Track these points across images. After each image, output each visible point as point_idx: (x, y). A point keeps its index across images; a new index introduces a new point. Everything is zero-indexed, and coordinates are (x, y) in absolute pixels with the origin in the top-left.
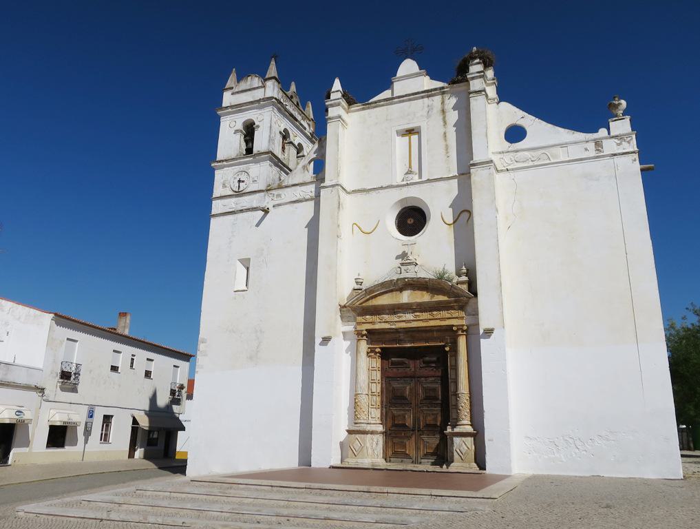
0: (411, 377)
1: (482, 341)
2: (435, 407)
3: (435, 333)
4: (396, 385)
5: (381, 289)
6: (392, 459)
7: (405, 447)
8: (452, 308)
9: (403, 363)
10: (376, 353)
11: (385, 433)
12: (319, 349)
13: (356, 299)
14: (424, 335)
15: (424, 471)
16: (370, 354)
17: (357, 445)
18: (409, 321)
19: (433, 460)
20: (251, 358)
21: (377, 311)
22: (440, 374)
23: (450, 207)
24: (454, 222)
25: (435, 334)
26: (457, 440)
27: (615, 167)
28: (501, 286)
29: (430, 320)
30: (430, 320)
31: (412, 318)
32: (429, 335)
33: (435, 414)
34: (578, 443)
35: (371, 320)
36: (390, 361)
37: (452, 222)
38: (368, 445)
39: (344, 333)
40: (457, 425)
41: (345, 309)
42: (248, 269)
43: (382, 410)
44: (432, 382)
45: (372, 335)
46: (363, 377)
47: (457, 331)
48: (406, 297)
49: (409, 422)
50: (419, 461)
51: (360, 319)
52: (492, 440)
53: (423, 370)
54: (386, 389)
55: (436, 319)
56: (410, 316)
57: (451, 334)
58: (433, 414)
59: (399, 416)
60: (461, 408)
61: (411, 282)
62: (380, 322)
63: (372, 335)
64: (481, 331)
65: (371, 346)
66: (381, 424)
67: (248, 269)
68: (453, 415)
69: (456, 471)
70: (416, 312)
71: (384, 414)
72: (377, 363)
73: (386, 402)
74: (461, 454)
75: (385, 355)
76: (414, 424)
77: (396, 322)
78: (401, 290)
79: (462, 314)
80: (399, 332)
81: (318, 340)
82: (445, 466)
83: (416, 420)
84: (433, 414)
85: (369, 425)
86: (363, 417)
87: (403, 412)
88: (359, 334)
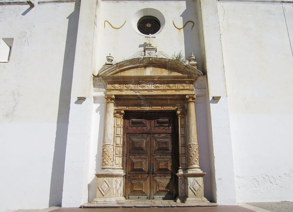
0: (147, 133)
1: (212, 105)
2: (166, 156)
3: (169, 101)
4: (135, 139)
5: (129, 65)
6: (130, 196)
7: (141, 186)
8: (184, 82)
9: (141, 123)
10: (121, 114)
11: (125, 177)
12: (73, 106)
13: (108, 71)
14: (160, 102)
15: (169, 207)
16: (116, 115)
17: (105, 186)
18: (151, 90)
19: (164, 196)
20: (7, 116)
21: (125, 81)
22: (170, 131)
23: (181, 16)
24: (184, 27)
25: (169, 102)
26: (190, 180)
27: (284, 10)
28: (224, 68)
29: (168, 90)
30: (168, 90)
31: (153, 88)
32: (163, 102)
33: (166, 161)
34: (272, 179)
35: (119, 88)
36: (130, 120)
37: (182, 26)
38: (114, 186)
39: (95, 98)
40: (188, 169)
41: (97, 79)
42: (11, 48)
43: (123, 158)
44: (164, 138)
45: (119, 100)
46: (110, 131)
47: (188, 99)
48: (149, 72)
49: (145, 168)
50: (152, 196)
51: (109, 86)
52: (221, 179)
53: (157, 128)
54: (127, 142)
55: (173, 90)
56: (151, 87)
57: (183, 100)
58: (164, 161)
59: (138, 162)
60: (192, 155)
61: (154, 61)
62: (127, 90)
63: (119, 100)
64: (211, 98)
65: (116, 108)
66: (122, 169)
67: (11, 48)
68: (182, 160)
69: (197, 204)
70: (157, 83)
71: (125, 161)
72: (120, 122)
73: (127, 152)
74: (194, 191)
75: (127, 116)
76: (149, 169)
77: (140, 90)
78: (145, 67)
79: (192, 86)
80: (141, 99)
81: (74, 99)
82: (178, 200)
83: (150, 165)
84: (164, 161)
85: (114, 170)
86: (109, 163)
87: (140, 160)
88: (108, 98)
